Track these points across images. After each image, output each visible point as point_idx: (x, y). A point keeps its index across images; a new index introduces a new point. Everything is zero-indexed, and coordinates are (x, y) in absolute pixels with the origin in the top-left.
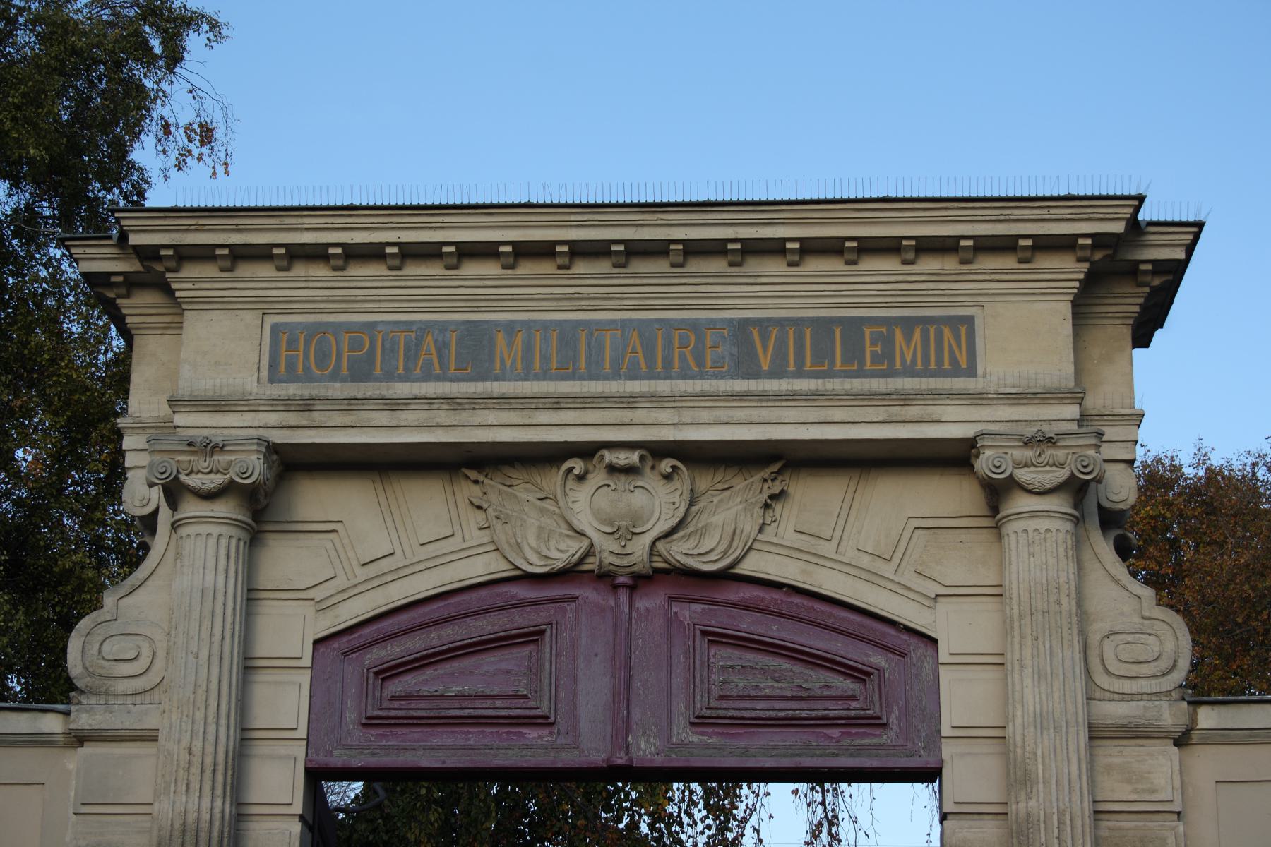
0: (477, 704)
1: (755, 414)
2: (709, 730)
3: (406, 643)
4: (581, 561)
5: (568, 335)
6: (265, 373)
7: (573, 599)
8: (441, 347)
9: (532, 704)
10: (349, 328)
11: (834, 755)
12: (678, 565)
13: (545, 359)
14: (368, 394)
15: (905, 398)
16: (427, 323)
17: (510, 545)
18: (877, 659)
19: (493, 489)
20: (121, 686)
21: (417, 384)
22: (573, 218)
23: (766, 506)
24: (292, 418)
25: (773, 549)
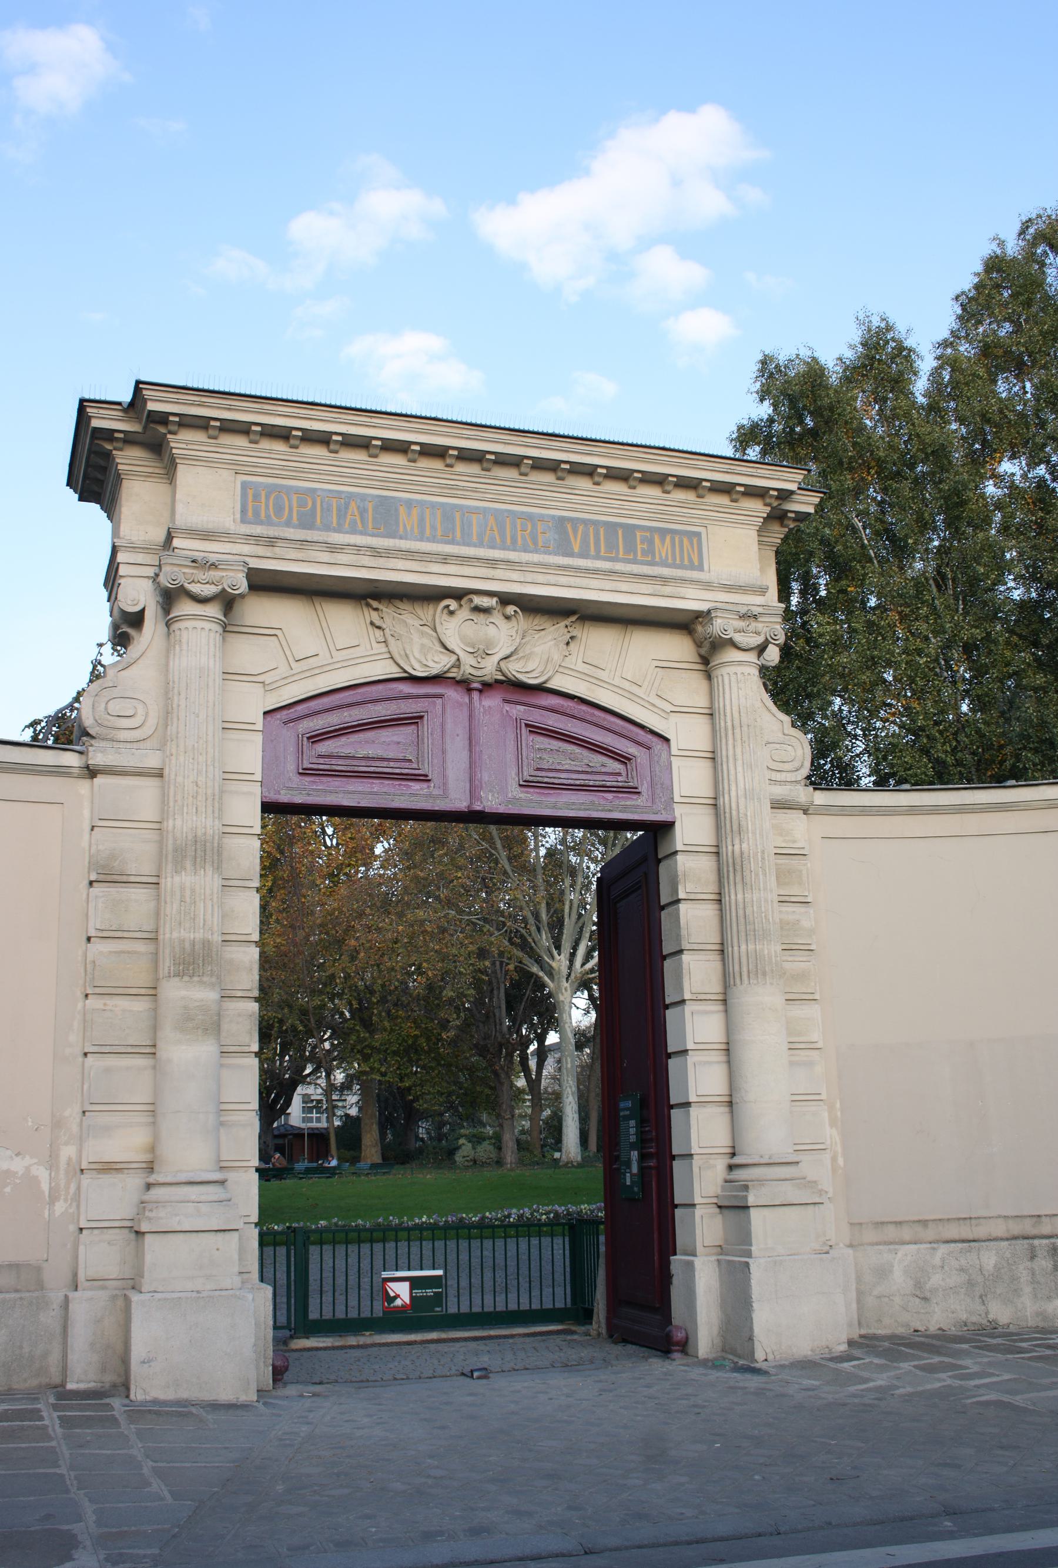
0: (378, 764)
1: (572, 581)
2: (532, 790)
3: (327, 719)
4: (446, 672)
5: (448, 513)
6: (238, 516)
7: (440, 696)
8: (363, 512)
9: (415, 766)
10: (298, 491)
11: (610, 811)
12: (513, 679)
13: (433, 528)
14: (315, 539)
15: (665, 580)
16: (351, 493)
17: (401, 656)
18: (632, 749)
19: (389, 615)
20: (123, 735)
21: (347, 536)
22: (464, 432)
23: (568, 644)
24: (261, 551)
25: (570, 673)
